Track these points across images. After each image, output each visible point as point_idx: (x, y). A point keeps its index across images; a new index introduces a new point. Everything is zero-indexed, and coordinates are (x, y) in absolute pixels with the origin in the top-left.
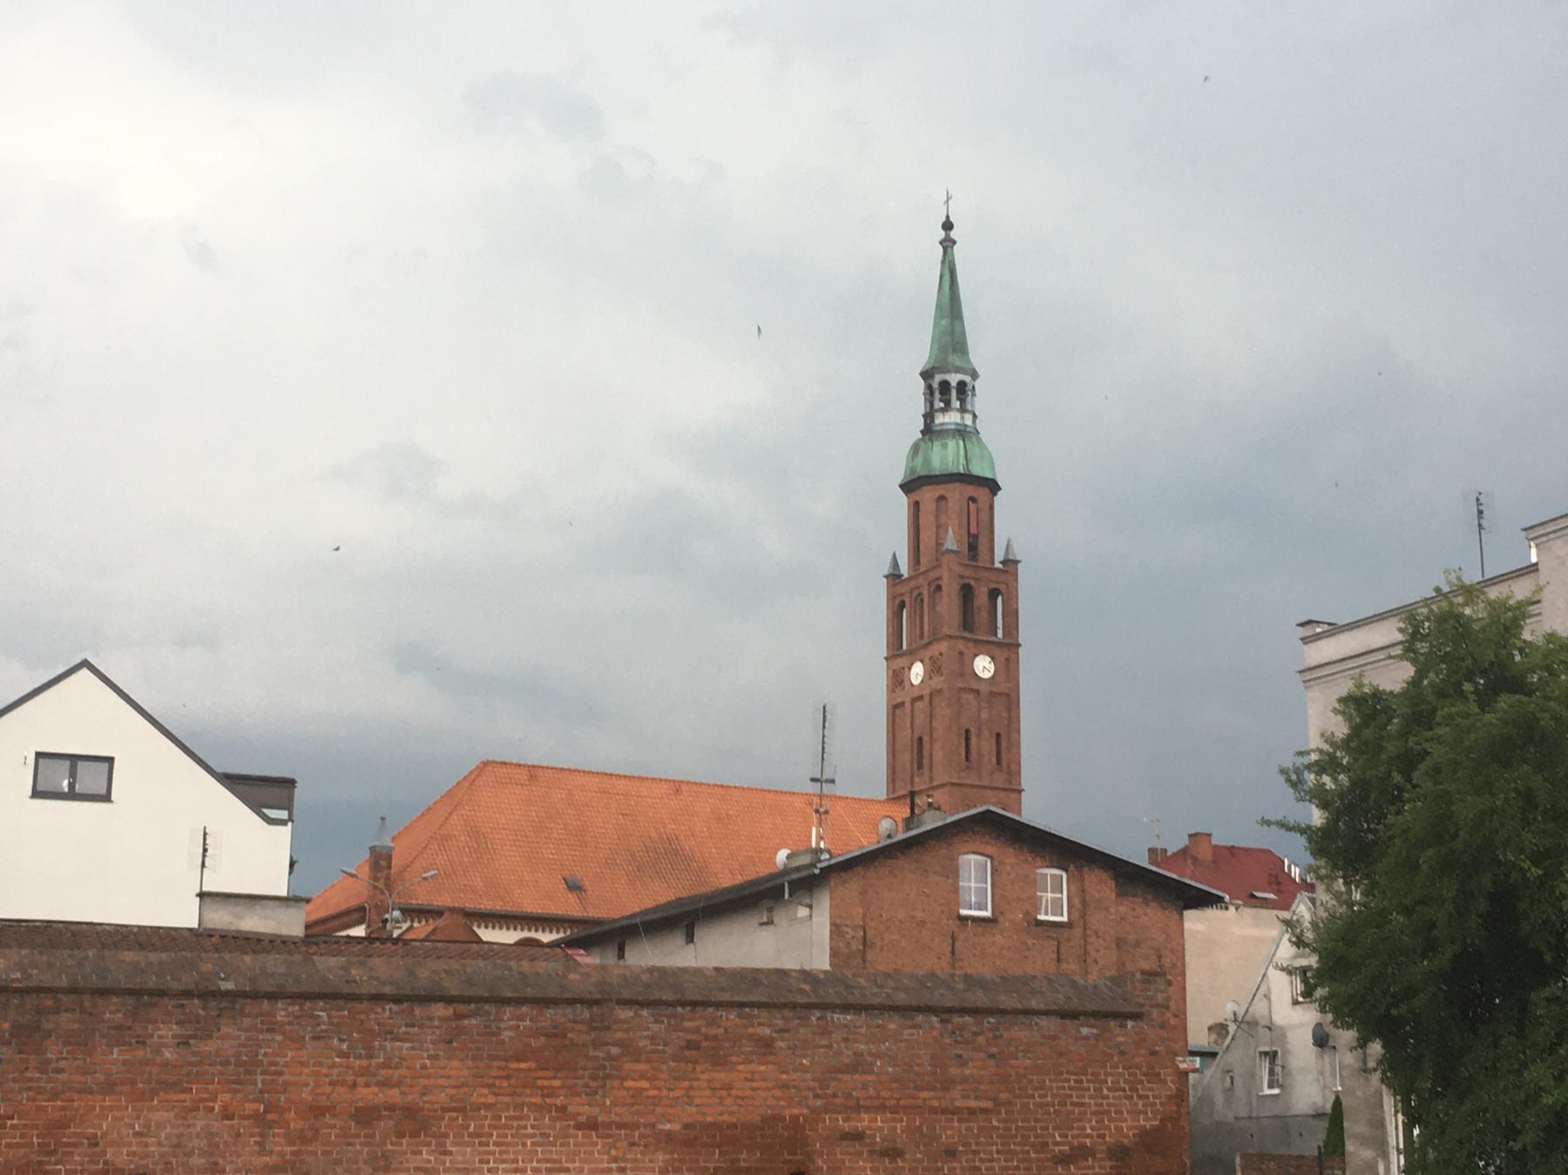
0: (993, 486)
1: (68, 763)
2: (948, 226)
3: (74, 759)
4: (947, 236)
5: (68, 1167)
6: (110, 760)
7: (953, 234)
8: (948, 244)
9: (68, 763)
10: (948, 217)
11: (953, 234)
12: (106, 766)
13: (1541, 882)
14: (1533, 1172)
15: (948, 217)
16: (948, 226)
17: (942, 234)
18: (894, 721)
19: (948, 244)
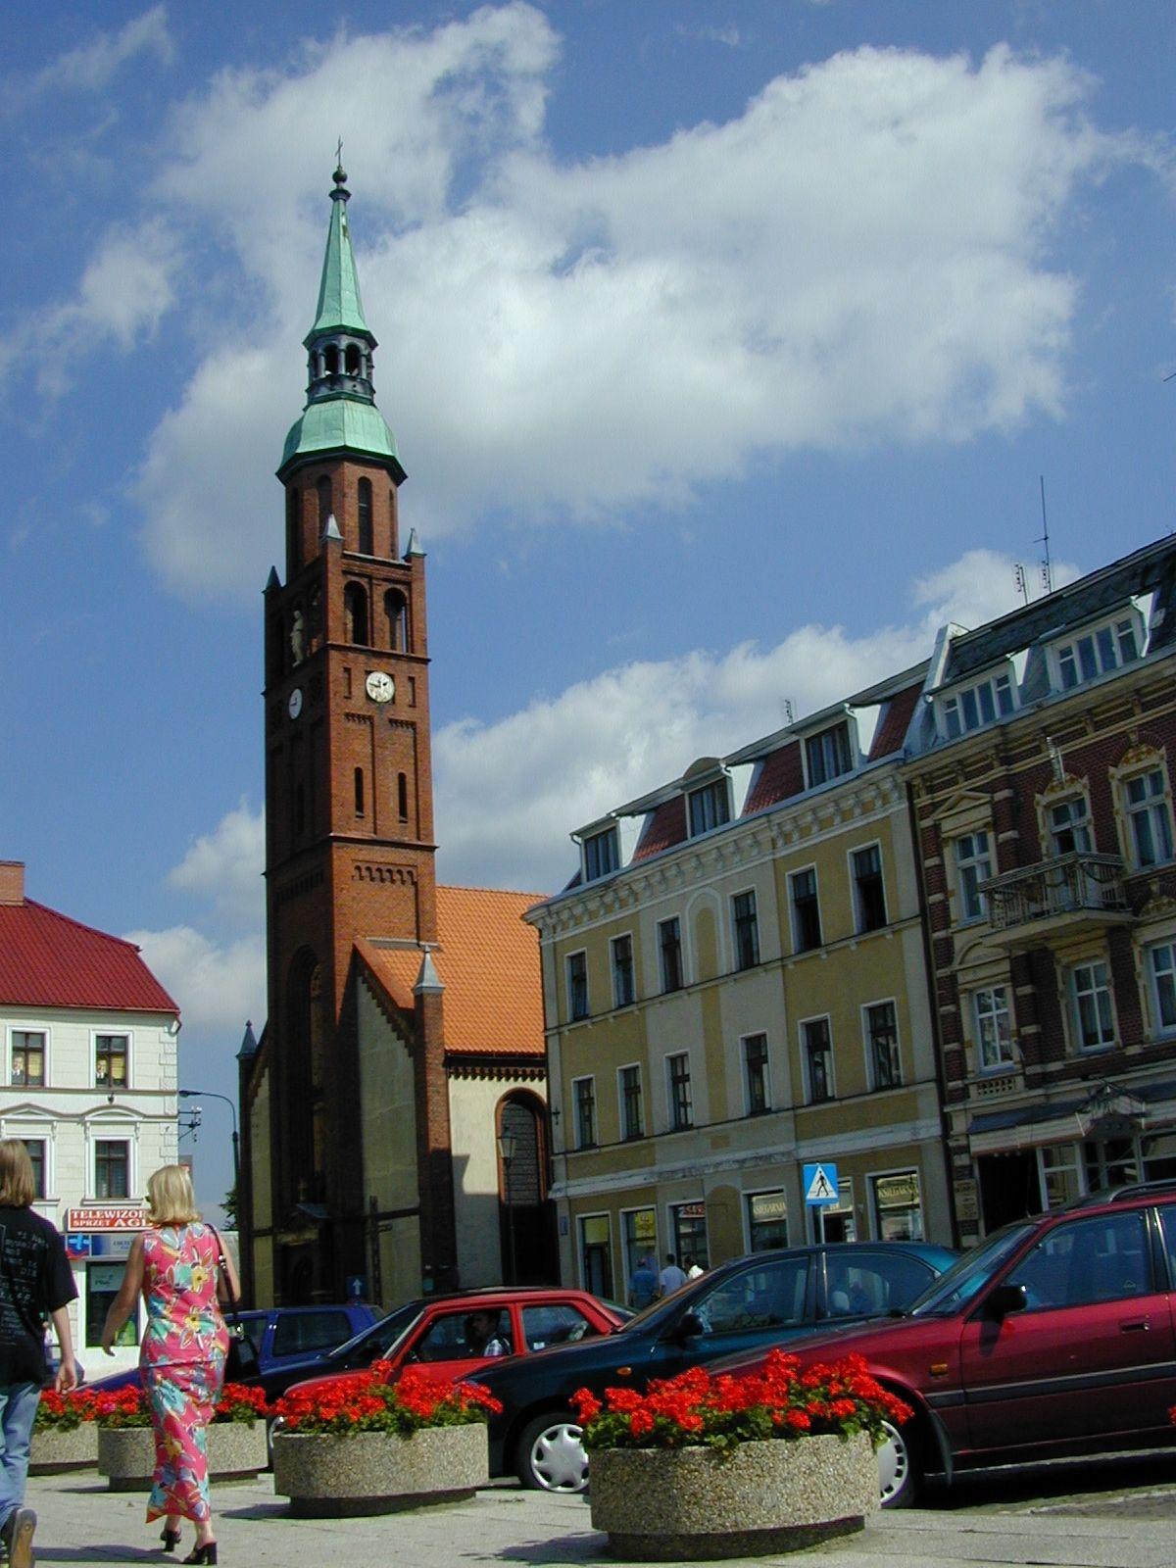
15: (339, 167)
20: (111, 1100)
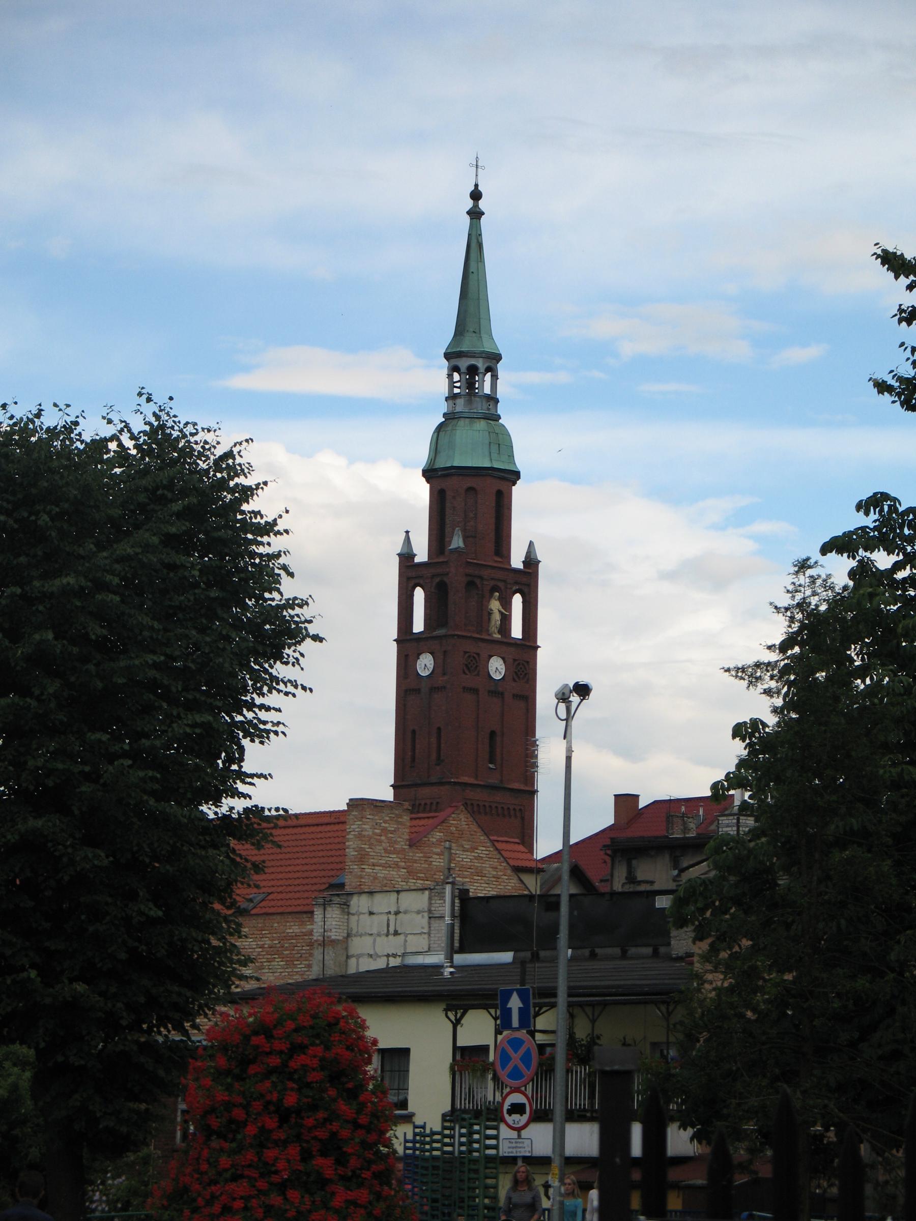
2: (476, 195)
4: (476, 206)
7: (482, 204)
8: (475, 214)
10: (476, 186)
15: (476, 186)
16: (476, 195)
17: (470, 203)
19: (475, 214)
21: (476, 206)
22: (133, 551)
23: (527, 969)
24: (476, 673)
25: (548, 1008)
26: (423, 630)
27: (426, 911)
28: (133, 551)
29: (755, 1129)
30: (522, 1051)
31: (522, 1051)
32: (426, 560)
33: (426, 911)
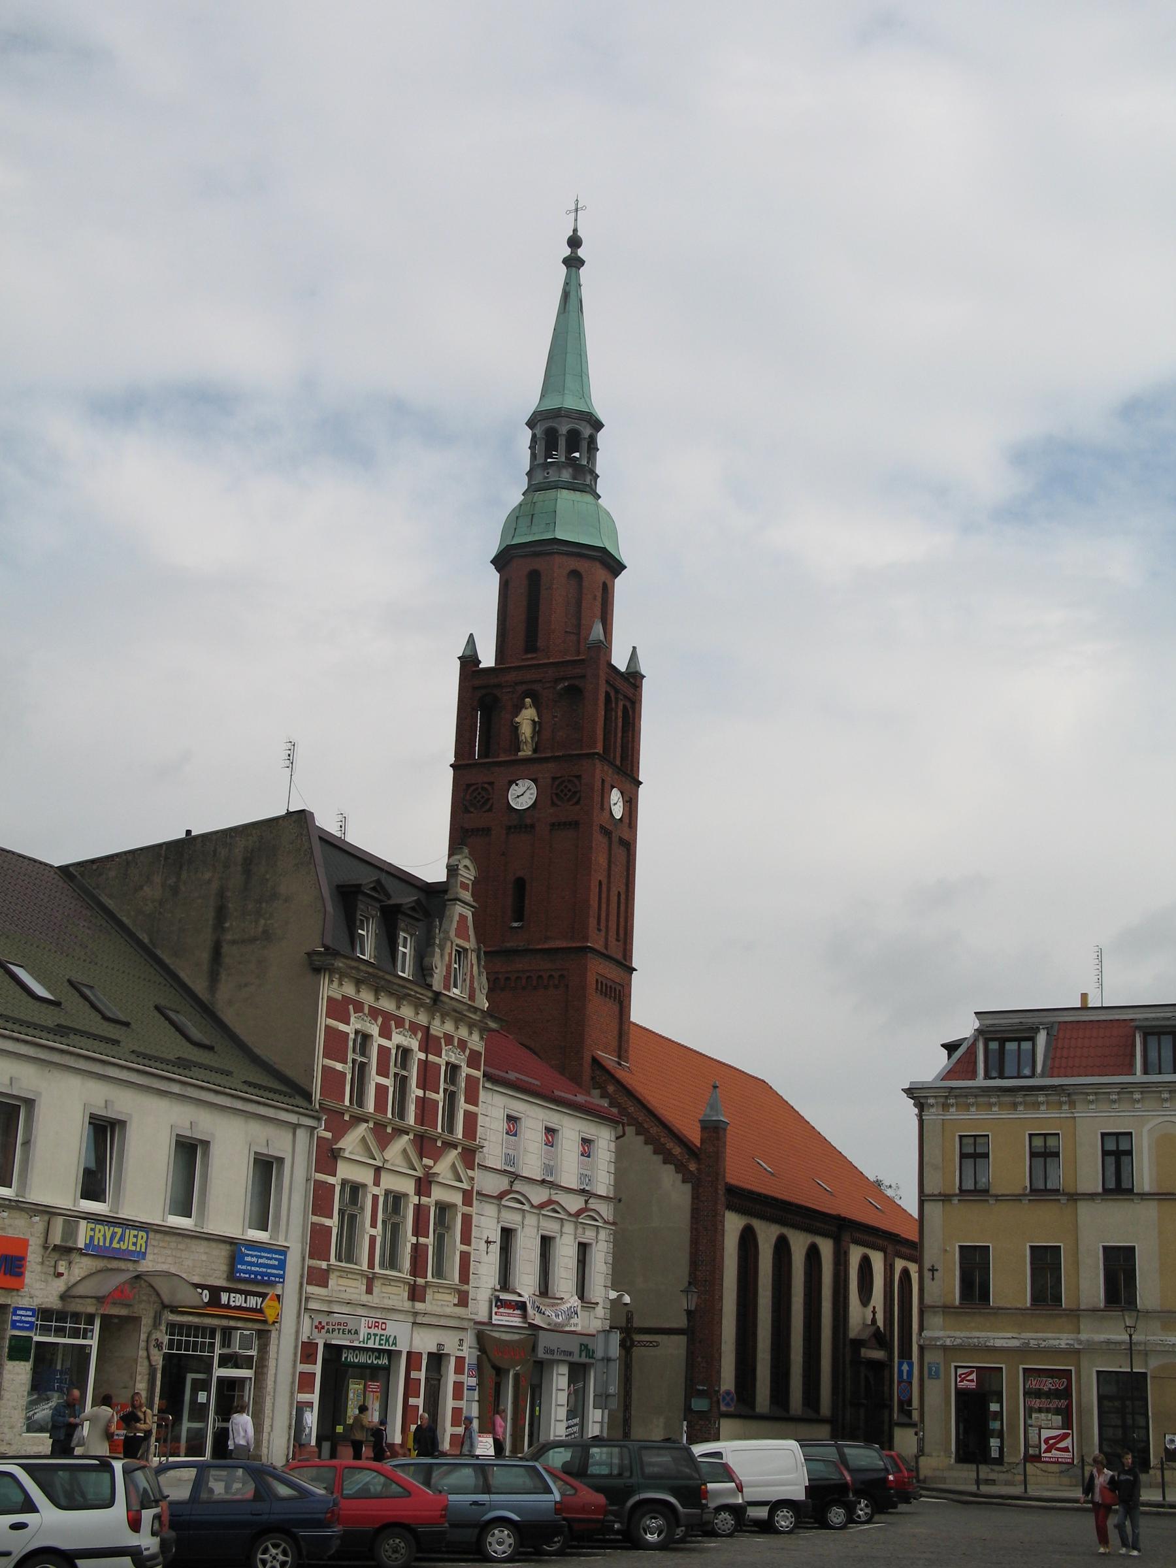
0: (616, 567)
1: (1115, 1137)
2: (574, 242)
3: (1117, 1135)
4: (574, 252)
5: (255, 1357)
6: (1130, 1134)
7: (581, 252)
8: (573, 263)
9: (1115, 1137)
10: (575, 230)
11: (581, 252)
12: (1129, 1137)
13: (603, 1087)
14: (1172, 1498)
15: (575, 230)
16: (574, 242)
17: (567, 251)
18: (425, 1075)
19: (573, 263)
20: (586, 1202)
21: (574, 252)
22: (148, 1433)
23: (251, 1306)
24: (575, 780)
25: (270, 1479)
26: (631, 1020)
27: (975, 1150)
28: (148, 1433)
29: (608, 1535)
30: (730, 1396)
31: (730, 1396)
32: (494, 665)
33: (975, 1150)
